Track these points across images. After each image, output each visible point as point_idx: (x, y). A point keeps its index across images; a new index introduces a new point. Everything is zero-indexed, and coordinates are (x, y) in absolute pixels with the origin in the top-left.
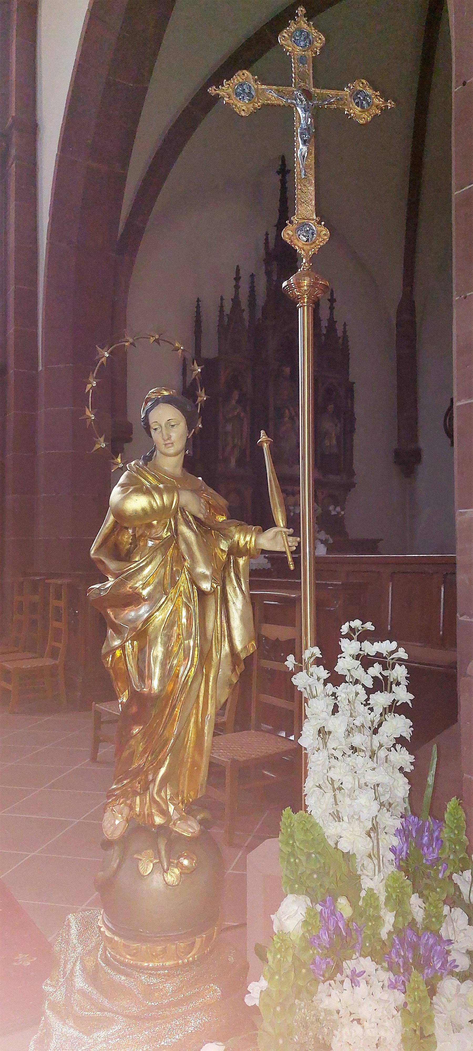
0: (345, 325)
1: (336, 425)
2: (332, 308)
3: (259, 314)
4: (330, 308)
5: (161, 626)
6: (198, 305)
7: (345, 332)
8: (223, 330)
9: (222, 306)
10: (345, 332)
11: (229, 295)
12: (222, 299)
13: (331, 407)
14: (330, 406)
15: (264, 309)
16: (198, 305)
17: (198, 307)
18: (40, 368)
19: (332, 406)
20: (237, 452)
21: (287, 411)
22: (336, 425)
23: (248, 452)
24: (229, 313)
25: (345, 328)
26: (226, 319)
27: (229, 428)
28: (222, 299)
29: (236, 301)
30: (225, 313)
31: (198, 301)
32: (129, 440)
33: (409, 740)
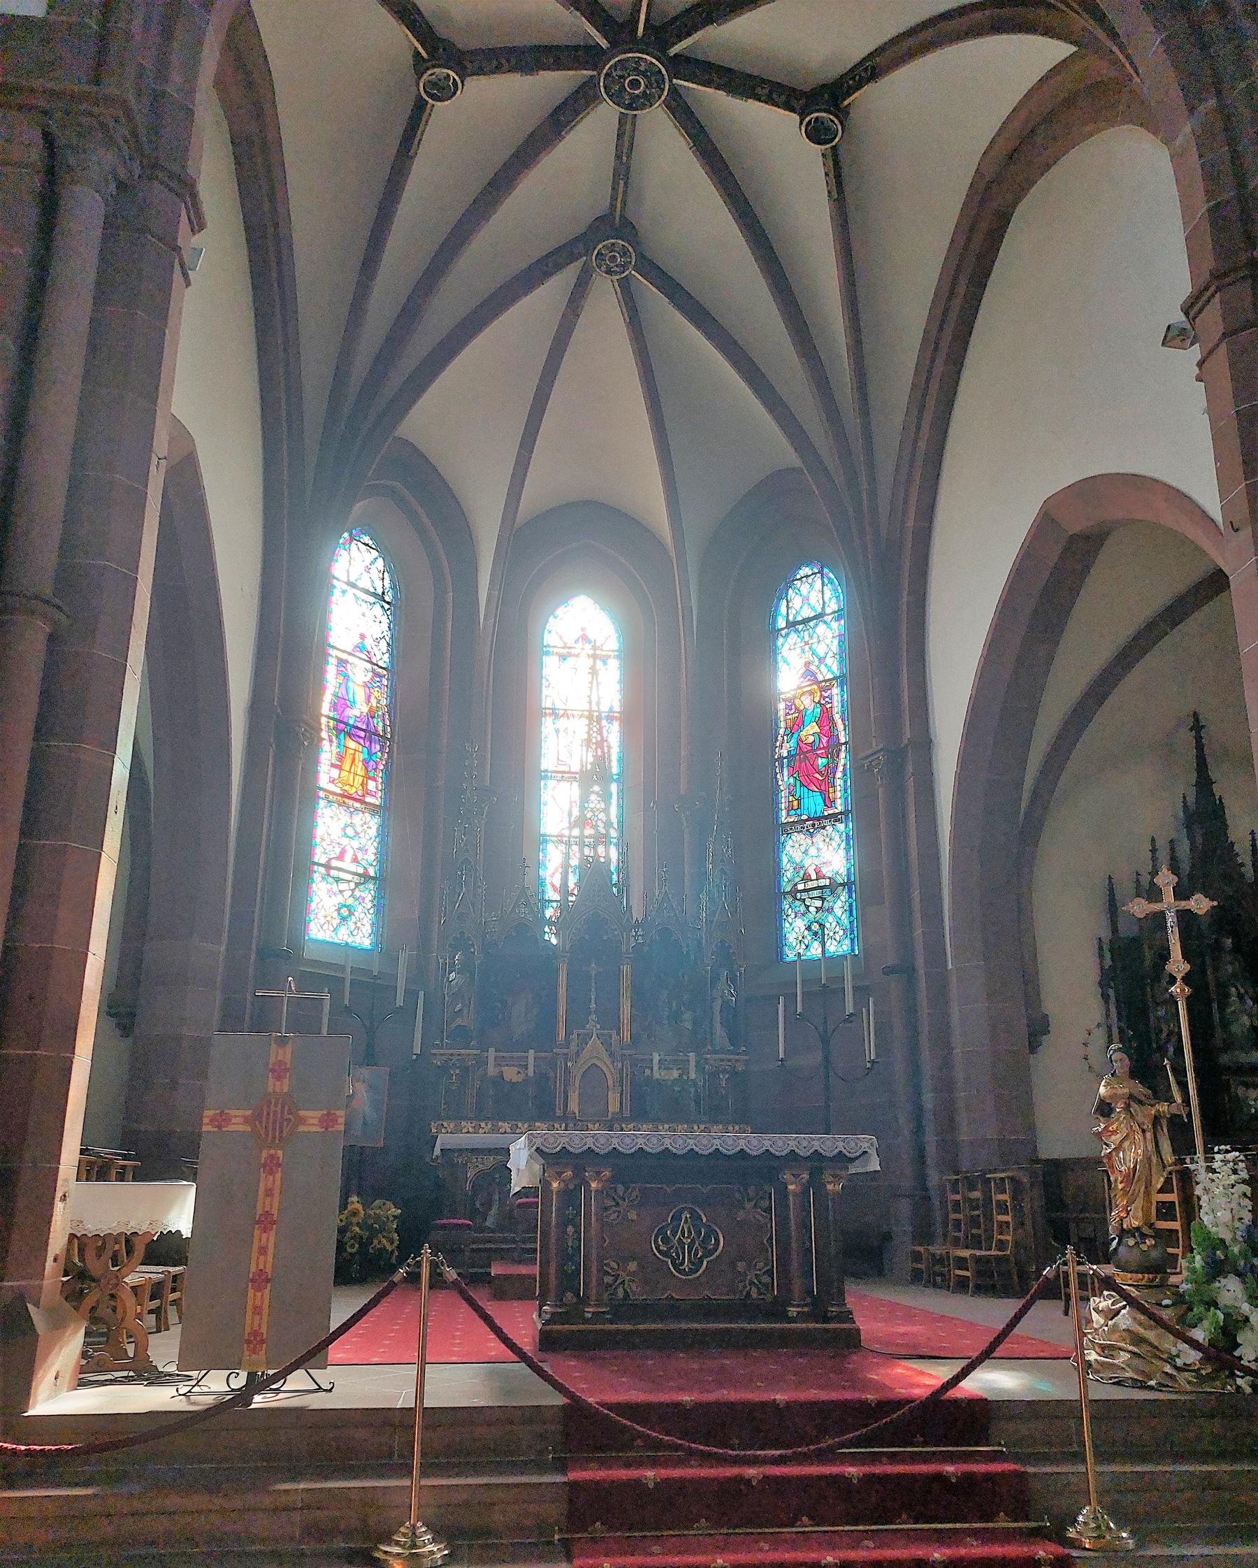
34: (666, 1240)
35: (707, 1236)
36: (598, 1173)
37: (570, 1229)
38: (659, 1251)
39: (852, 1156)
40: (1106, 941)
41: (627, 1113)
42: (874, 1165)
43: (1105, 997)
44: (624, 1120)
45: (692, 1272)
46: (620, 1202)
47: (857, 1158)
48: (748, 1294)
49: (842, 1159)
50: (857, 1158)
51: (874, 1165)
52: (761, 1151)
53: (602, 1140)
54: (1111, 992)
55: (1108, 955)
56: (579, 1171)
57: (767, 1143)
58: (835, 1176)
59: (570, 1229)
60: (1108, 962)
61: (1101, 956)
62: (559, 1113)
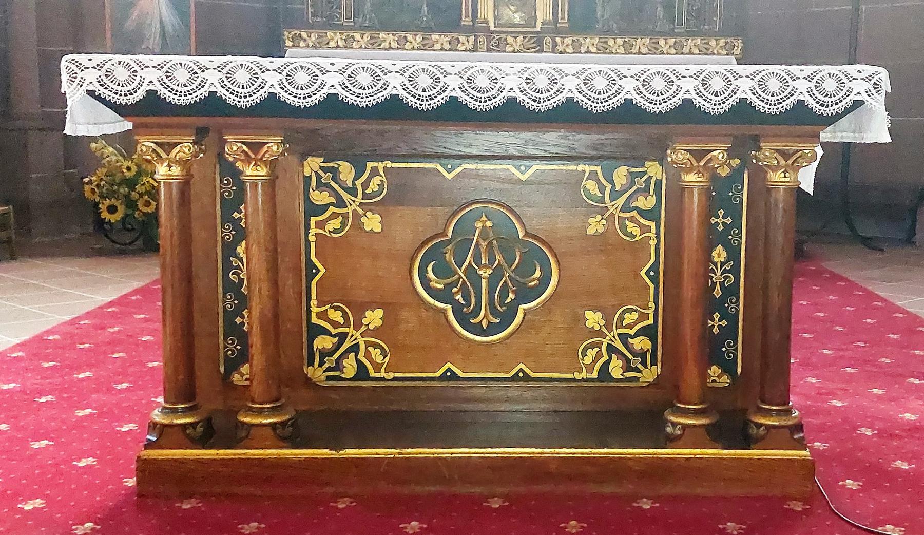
34: (443, 271)
35: (525, 269)
36: (256, 147)
37: (719, 254)
38: (428, 288)
39: (830, 111)
41: (563, 23)
42: (878, 130)
44: (557, 31)
45: (492, 329)
46: (346, 197)
47: (838, 116)
48: (605, 371)
49: (802, 119)
50: (838, 116)
51: (878, 130)
52: (787, 104)
53: (717, 84)
56: (743, 147)
57: (802, 86)
58: (785, 155)
59: (719, 254)
62: (466, 21)
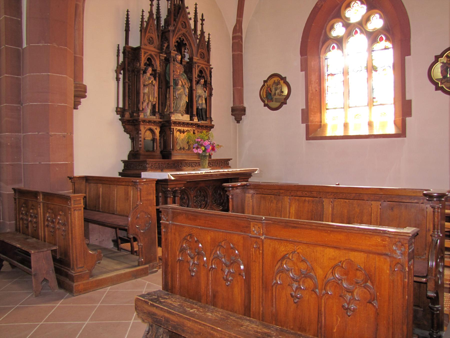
0: (209, 35)
1: (205, 92)
2: (202, 24)
3: (162, 23)
4: (203, 24)
5: (240, 235)
6: (196, 7)
7: (209, 38)
8: (143, 30)
9: (143, 16)
10: (209, 38)
11: (147, 9)
12: (143, 11)
13: (202, 81)
14: (201, 80)
15: (166, 21)
16: (196, 7)
17: (128, 15)
18: (25, 45)
19: (203, 80)
20: (150, 107)
21: (180, 82)
22: (205, 92)
23: (157, 106)
24: (147, 20)
25: (209, 37)
26: (145, 23)
27: (146, 91)
28: (143, 11)
29: (151, 13)
30: (145, 20)
31: (128, 11)
32: (85, 97)
33: (369, 281)
40: (121, 50)
43: (118, 79)
54: (121, 76)
55: (121, 55)
60: (121, 59)
61: (118, 56)
